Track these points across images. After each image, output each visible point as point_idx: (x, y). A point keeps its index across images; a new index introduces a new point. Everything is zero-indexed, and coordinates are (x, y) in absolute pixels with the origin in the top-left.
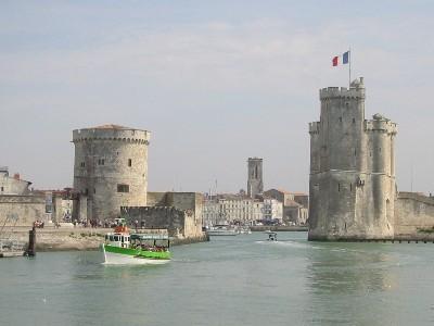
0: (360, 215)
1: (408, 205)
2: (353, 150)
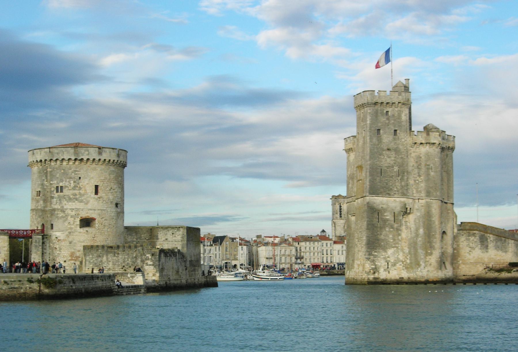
0: (407, 250)
1: (472, 238)
2: (396, 169)
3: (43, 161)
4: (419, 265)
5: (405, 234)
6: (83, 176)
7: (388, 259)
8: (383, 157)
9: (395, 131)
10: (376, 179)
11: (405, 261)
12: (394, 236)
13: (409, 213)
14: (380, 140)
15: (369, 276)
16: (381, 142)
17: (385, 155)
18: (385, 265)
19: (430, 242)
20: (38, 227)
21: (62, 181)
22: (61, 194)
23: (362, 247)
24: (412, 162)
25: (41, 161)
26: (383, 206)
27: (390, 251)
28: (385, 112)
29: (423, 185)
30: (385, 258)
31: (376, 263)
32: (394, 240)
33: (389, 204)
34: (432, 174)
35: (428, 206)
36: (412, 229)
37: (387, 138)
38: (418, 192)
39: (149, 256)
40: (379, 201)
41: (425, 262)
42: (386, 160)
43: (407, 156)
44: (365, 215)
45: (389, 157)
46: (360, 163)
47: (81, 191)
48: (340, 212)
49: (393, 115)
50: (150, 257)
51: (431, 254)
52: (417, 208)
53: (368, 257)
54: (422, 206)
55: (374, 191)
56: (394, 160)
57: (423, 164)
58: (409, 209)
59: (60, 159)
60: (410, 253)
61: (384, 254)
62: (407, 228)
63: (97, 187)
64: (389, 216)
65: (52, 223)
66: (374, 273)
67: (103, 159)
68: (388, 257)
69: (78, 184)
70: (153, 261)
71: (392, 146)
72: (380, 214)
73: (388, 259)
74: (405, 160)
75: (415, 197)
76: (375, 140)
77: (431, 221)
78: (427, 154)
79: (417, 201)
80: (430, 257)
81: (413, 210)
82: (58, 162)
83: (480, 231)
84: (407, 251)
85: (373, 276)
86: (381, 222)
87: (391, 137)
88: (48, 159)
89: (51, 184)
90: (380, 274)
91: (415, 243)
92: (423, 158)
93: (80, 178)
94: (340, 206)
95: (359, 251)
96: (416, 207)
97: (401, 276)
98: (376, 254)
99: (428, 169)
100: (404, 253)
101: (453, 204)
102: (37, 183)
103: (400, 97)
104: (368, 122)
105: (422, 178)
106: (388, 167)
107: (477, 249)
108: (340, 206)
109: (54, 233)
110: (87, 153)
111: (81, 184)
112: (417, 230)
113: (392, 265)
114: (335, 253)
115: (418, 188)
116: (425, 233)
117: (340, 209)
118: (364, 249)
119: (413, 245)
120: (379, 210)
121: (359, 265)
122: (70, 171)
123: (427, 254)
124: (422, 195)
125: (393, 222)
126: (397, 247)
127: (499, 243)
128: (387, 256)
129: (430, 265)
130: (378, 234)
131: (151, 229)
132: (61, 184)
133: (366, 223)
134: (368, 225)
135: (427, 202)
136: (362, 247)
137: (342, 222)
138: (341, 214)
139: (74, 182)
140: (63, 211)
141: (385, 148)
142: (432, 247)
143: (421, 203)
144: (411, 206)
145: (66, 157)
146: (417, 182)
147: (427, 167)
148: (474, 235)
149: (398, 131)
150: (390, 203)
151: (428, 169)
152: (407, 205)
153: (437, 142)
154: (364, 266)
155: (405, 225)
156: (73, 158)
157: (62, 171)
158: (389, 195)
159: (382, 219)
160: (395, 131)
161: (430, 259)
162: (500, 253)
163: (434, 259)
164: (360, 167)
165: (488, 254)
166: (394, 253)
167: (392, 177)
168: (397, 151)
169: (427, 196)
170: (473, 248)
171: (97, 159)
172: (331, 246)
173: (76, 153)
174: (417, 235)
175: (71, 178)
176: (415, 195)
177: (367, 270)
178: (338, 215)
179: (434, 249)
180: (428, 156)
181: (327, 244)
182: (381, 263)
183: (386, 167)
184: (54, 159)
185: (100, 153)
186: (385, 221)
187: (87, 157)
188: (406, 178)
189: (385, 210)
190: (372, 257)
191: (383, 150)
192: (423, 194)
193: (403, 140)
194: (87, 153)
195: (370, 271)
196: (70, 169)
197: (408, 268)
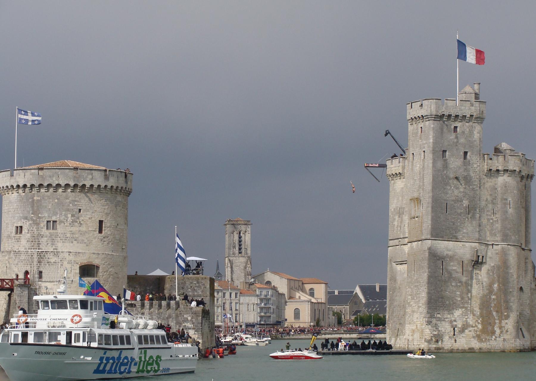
0: (478, 311)
2: (465, 203)
3: (29, 186)
4: (493, 332)
5: (476, 291)
6: (84, 208)
7: (455, 323)
8: (449, 188)
9: (466, 153)
10: (439, 217)
11: (476, 326)
12: (462, 293)
13: (482, 263)
14: (446, 166)
15: (430, 346)
16: (447, 167)
17: (452, 185)
18: (451, 332)
19: (507, 302)
20: (17, 276)
21: (55, 214)
22: (54, 231)
23: (419, 307)
24: (485, 195)
25: (25, 186)
26: (448, 252)
27: (458, 313)
28: (453, 127)
29: (498, 226)
30: (451, 322)
31: (440, 329)
32: (462, 298)
33: (457, 251)
34: (510, 211)
35: (504, 254)
36: (484, 284)
37: (455, 162)
38: (492, 234)
40: (444, 246)
41: (501, 328)
42: (453, 191)
43: (480, 187)
44: (425, 264)
45: (457, 188)
46: (416, 195)
47: (81, 228)
48: (240, 245)
49: (463, 132)
50: (189, 318)
51: (507, 317)
52: (491, 256)
53: (430, 320)
54: (497, 254)
55: (437, 233)
56: (463, 192)
57: (499, 197)
58: (480, 258)
59: (54, 185)
60: (481, 315)
61: (449, 316)
62: (478, 282)
63: (101, 222)
64: (454, 267)
65: (41, 269)
66: (437, 341)
67: (109, 187)
68: (455, 321)
69: (78, 218)
70: (193, 324)
71: (461, 173)
72: (444, 263)
73: (455, 323)
74: (478, 192)
75: (488, 241)
77: (508, 273)
78: (505, 186)
79: (491, 247)
80: (506, 321)
81: (486, 259)
82: (51, 190)
84: (479, 313)
85: (434, 346)
88: (37, 184)
89: (40, 218)
90: (444, 343)
92: (499, 189)
93: (80, 210)
94: (240, 237)
95: (413, 312)
96: (489, 254)
97: (470, 346)
98: (439, 316)
99: (505, 204)
100: (474, 315)
101: (530, 250)
102: (18, 215)
103: (473, 108)
104: (431, 141)
105: (497, 216)
108: (240, 237)
109: (43, 285)
110: (90, 177)
111: (81, 219)
112: (491, 285)
113: (460, 331)
114: (243, 308)
115: (492, 230)
116: (499, 289)
117: (240, 241)
118: (423, 309)
119: (485, 304)
120: (444, 259)
121: (413, 331)
122: (68, 201)
124: (497, 239)
125: (460, 275)
126: (466, 308)
128: (453, 319)
129: (507, 331)
130: (442, 290)
132: (54, 218)
133: (426, 274)
134: (429, 277)
135: (503, 248)
136: (419, 307)
137: (242, 260)
138: (240, 249)
139: (73, 216)
140: (56, 253)
141: (452, 176)
142: (508, 308)
143: (496, 250)
144: (484, 253)
145: (63, 183)
146: (491, 221)
147: (504, 201)
149: (468, 154)
150: (462, 249)
151: (505, 204)
152: (479, 252)
153: (518, 170)
154: (422, 331)
155: (476, 279)
156: (72, 184)
157: (56, 201)
159: (447, 270)
161: (506, 323)
163: (510, 324)
164: (417, 200)
166: (462, 314)
167: (460, 214)
168: (468, 180)
169: (503, 241)
171: (103, 186)
172: (236, 297)
174: (491, 291)
175: (68, 210)
176: (488, 239)
177: (428, 338)
178: (237, 250)
179: (512, 311)
180: (506, 187)
183: (453, 200)
184: (45, 184)
185: (106, 178)
187: (91, 183)
188: (478, 215)
189: (452, 258)
190: (434, 321)
191: (450, 179)
192: (498, 238)
193: (475, 166)
194: (90, 177)
195: (432, 339)
196: (67, 199)
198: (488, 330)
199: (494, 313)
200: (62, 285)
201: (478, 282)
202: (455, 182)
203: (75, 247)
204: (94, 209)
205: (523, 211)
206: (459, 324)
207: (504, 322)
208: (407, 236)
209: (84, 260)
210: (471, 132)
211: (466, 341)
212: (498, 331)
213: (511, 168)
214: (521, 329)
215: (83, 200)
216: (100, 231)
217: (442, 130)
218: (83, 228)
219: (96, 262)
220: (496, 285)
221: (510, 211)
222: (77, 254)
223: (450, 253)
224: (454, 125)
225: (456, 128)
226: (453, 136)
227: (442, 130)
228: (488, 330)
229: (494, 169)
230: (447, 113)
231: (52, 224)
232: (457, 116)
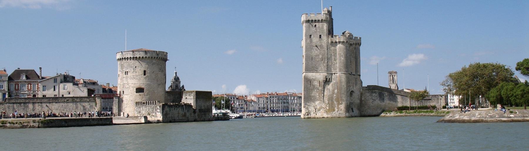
0: (327, 102)
1: (374, 94)
2: (321, 56)
4: (334, 110)
14: (311, 41)
21: (127, 69)
27: (317, 103)
30: (314, 107)
39: (158, 107)
40: (311, 75)
51: (341, 104)
60: (328, 103)
64: (316, 83)
66: (308, 115)
71: (318, 44)
76: (308, 41)
83: (379, 90)
86: (312, 87)
87: (318, 39)
91: (332, 98)
96: (333, 77)
106: (316, 56)
107: (377, 100)
112: (333, 91)
116: (338, 92)
119: (331, 99)
123: (339, 104)
127: (391, 97)
131: (307, 82)
148: (375, 92)
158: (317, 72)
160: (320, 36)
162: (392, 102)
165: (384, 103)
170: (375, 100)
173: (134, 55)
174: (333, 93)
181: (72, 116)
182: (312, 109)
186: (314, 86)
189: (314, 80)
190: (306, 106)
197: (327, 112)
198: (332, 109)
199: (335, 102)
200: (86, 91)
201: (327, 89)
202: (316, 48)
203: (134, 81)
204: (140, 67)
205: (353, 60)
206: (318, 107)
207: (340, 106)
208: (119, 62)
209: (138, 86)
210: (323, 27)
211: (322, 114)
212: (336, 110)
213: (342, 40)
214: (352, 109)
215: (136, 63)
216: (145, 74)
217: (309, 26)
218: (137, 74)
219: (143, 87)
220: (336, 91)
221: (342, 59)
222: (134, 84)
223: (314, 78)
224: (314, 24)
225: (315, 25)
226: (314, 29)
227: (309, 26)
228: (332, 109)
229: (334, 41)
230: (311, 19)
231: (126, 73)
232: (315, 20)
